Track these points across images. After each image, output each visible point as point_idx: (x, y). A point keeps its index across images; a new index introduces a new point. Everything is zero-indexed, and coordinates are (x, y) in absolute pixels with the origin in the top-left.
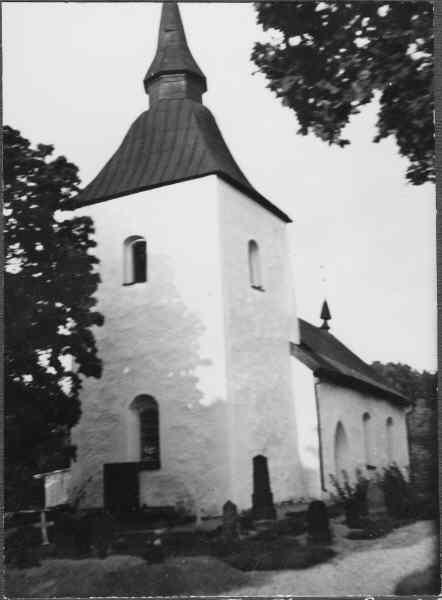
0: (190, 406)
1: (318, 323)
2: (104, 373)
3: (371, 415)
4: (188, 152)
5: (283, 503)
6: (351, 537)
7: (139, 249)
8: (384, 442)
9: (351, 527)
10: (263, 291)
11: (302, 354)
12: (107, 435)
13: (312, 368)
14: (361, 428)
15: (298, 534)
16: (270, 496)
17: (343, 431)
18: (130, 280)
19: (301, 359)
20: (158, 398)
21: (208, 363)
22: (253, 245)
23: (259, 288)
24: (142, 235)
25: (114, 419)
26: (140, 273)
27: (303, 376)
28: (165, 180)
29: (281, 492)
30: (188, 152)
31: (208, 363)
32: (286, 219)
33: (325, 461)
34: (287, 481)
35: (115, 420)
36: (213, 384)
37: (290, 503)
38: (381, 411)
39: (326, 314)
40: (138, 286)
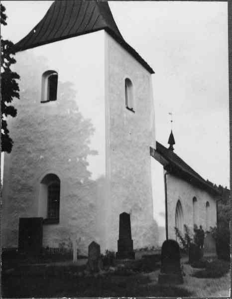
0: (82, 181)
1: (167, 146)
2: (13, 148)
3: (198, 200)
4: (87, 18)
5: (141, 250)
6: (198, 275)
7: (52, 78)
8: (204, 216)
9: (194, 266)
10: (134, 112)
11: (158, 155)
12: (25, 200)
13: (163, 164)
14: (192, 205)
15: (151, 271)
16: (131, 242)
17: (180, 204)
18: (46, 99)
19: (156, 158)
20: (59, 175)
21: (95, 153)
22: (128, 82)
23: (131, 110)
24: (56, 70)
25: (30, 189)
26: (53, 95)
27: (157, 170)
28: (71, 33)
29: (139, 242)
30: (87, 18)
31: (95, 153)
32: (151, 71)
33: (169, 225)
34: (145, 235)
35: (31, 191)
36: (97, 167)
37: (146, 249)
38: (204, 198)
39: (172, 141)
40: (52, 103)
